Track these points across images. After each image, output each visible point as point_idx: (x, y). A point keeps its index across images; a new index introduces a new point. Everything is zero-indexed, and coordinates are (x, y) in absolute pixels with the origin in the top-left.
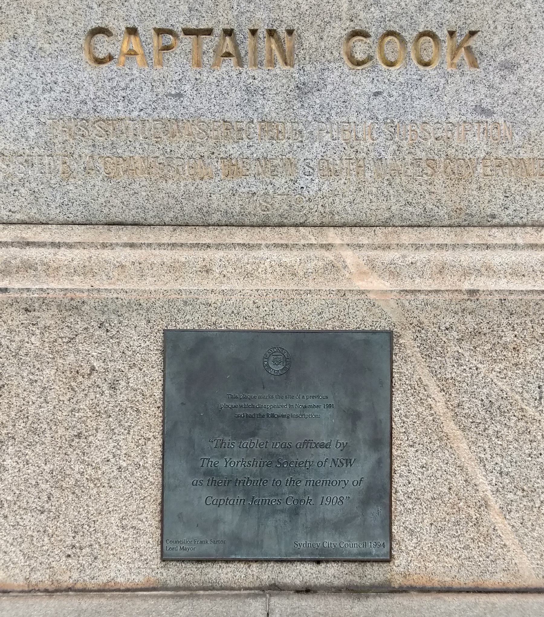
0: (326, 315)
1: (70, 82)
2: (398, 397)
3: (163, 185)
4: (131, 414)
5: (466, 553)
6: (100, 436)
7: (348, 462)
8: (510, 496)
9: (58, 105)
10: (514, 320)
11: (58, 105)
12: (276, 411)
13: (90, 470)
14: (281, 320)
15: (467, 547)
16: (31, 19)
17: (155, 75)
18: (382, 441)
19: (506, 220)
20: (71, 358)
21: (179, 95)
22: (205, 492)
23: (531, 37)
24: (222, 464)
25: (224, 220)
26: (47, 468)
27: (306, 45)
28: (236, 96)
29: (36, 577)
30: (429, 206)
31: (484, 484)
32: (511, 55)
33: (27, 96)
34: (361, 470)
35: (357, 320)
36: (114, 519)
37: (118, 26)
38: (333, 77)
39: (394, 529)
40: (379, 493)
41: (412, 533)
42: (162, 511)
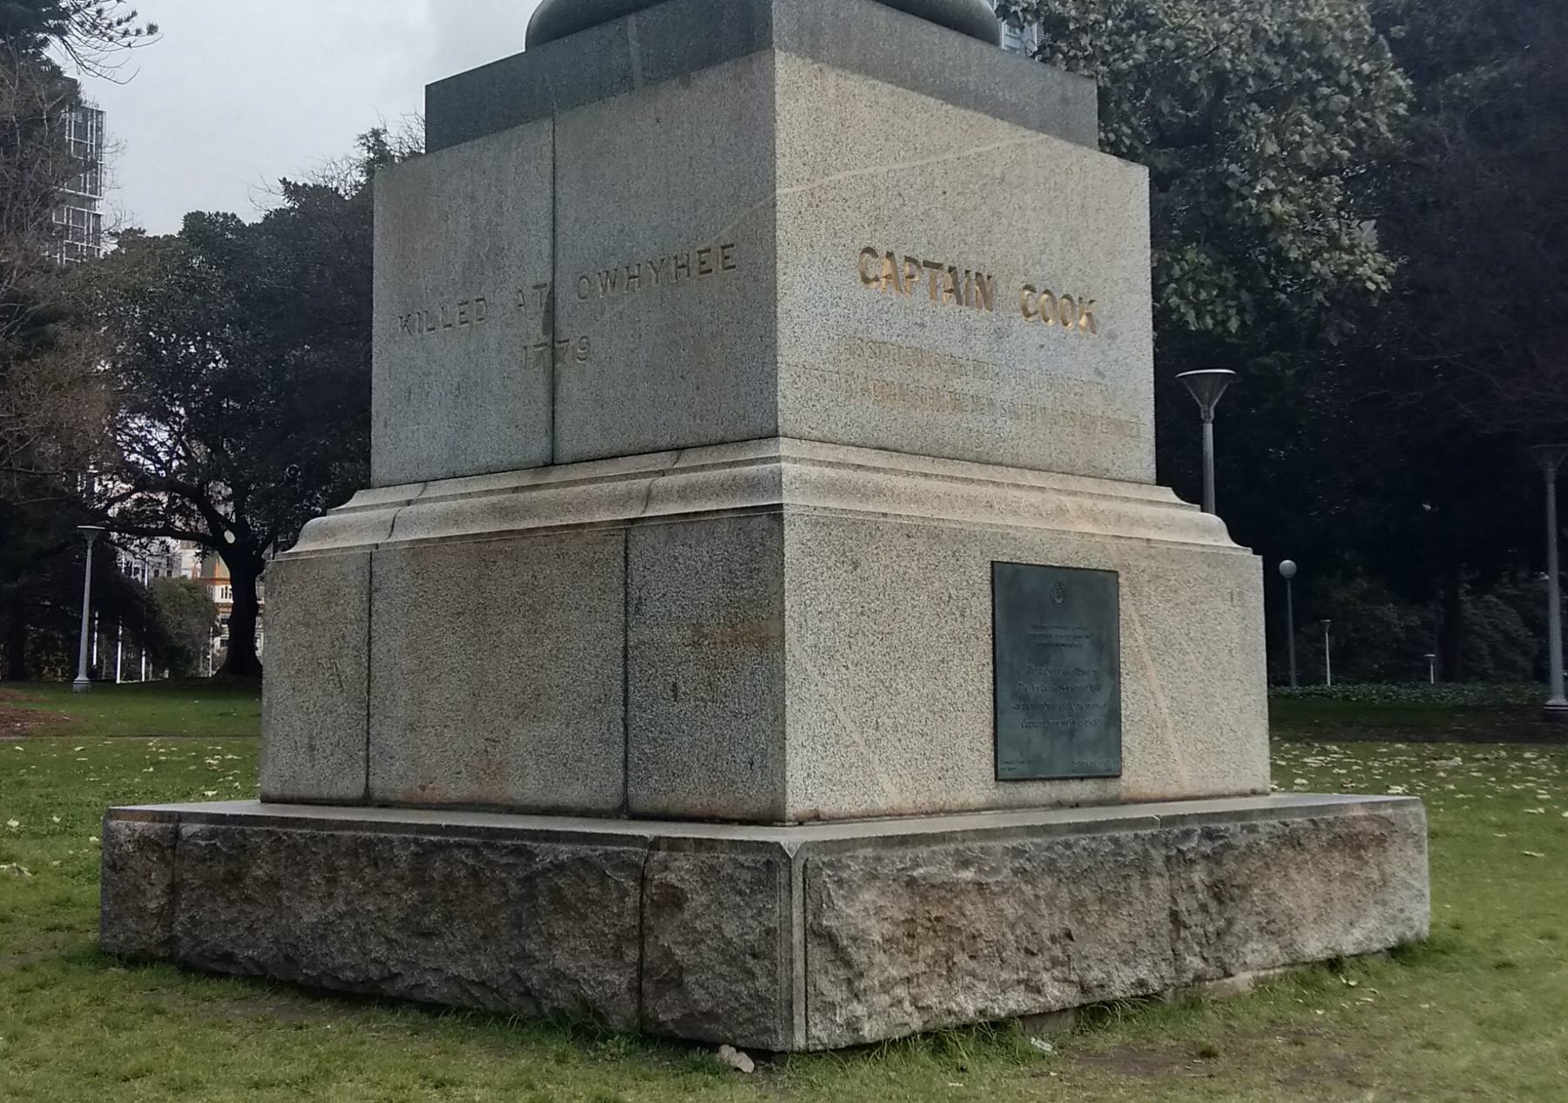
4: (973, 641)
12: (1061, 641)
14: (1055, 558)
18: (1114, 672)
29: (921, 799)
33: (820, 309)
34: (1101, 699)
37: (882, 250)
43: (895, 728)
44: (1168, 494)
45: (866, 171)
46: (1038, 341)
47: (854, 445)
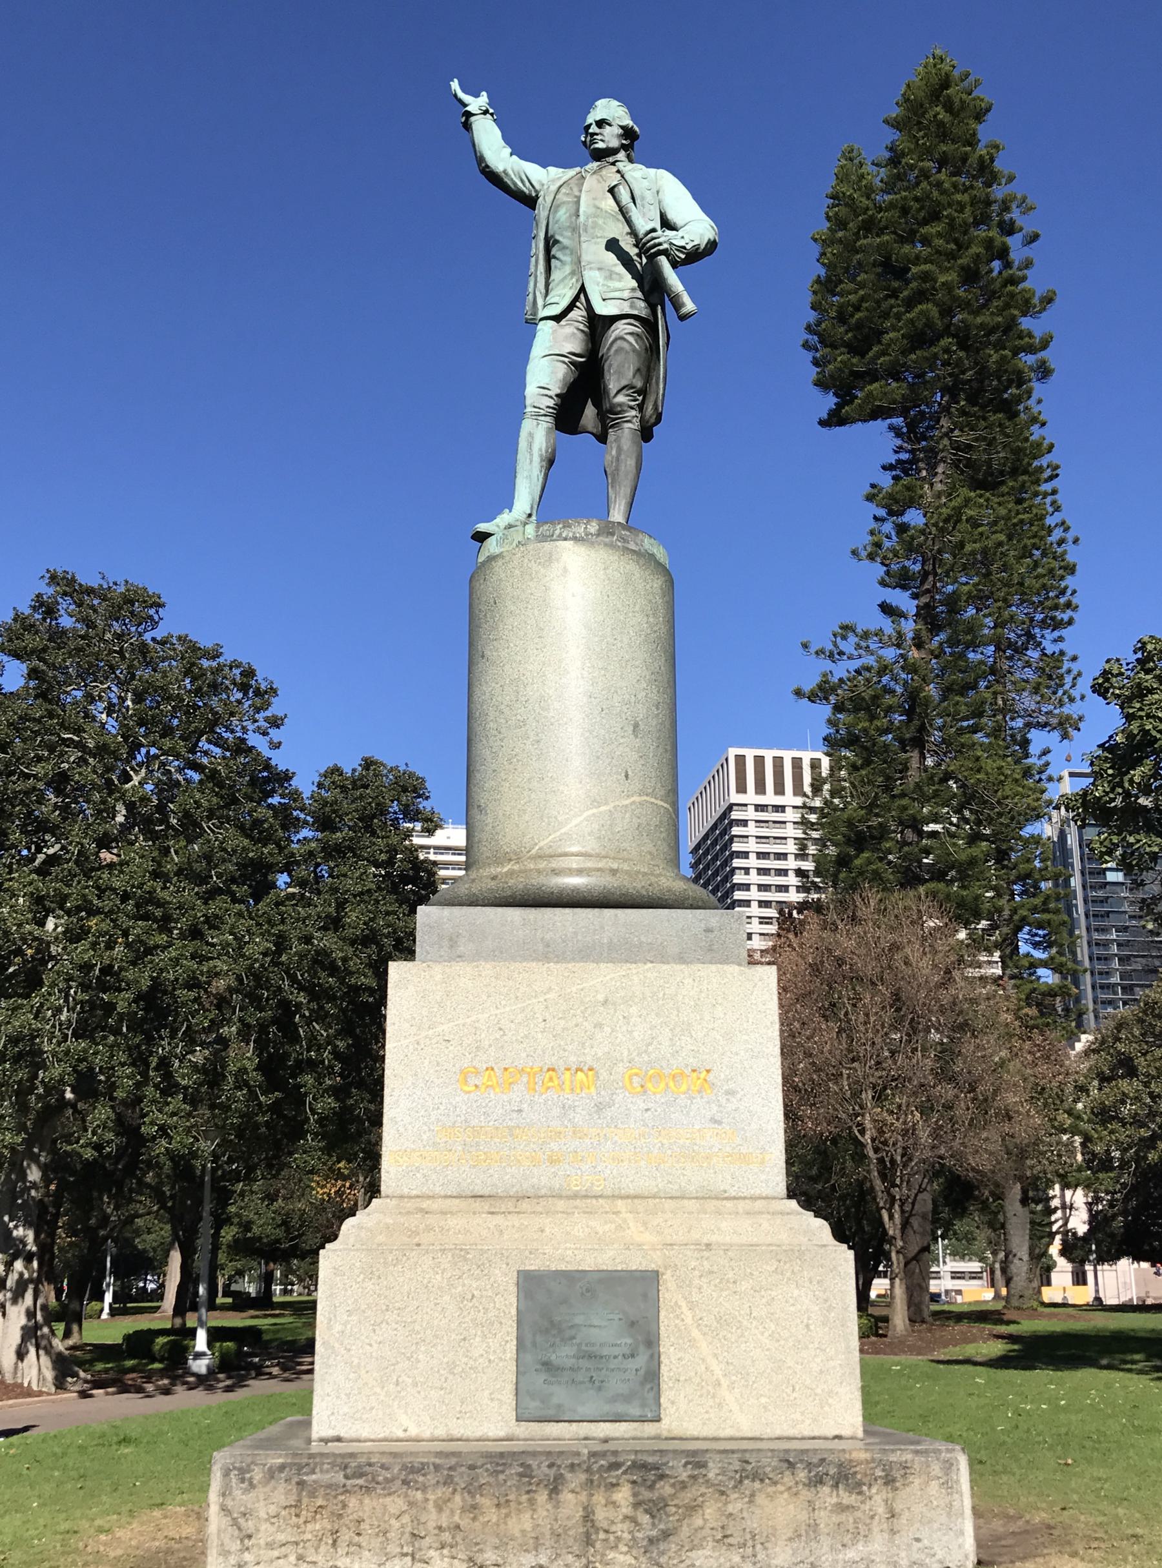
0: (617, 1261)
1: (451, 1103)
2: (662, 1314)
3: (508, 1170)
5: (707, 1416)
6: (478, 1339)
7: (633, 1356)
8: (734, 1378)
9: (442, 1118)
10: (732, 1263)
11: (442, 1118)
13: (471, 1362)
15: (707, 1412)
16: (426, 1062)
17: (505, 1098)
19: (734, 1194)
20: (460, 1288)
21: (520, 1111)
22: (543, 1376)
23: (745, 1074)
24: (553, 1357)
25: (549, 1193)
26: (445, 1360)
27: (601, 1078)
28: (556, 1111)
30: (683, 1184)
31: (718, 1370)
32: (732, 1085)
33: (422, 1113)
34: (641, 1361)
35: (636, 1263)
36: (486, 1393)
38: (618, 1098)
39: (662, 1400)
40: (652, 1377)
41: (673, 1403)
42: (516, 1389)
43: (415, 1384)
44: (793, 1204)
45: (468, 1021)
46: (643, 1106)
47: (450, 1197)
